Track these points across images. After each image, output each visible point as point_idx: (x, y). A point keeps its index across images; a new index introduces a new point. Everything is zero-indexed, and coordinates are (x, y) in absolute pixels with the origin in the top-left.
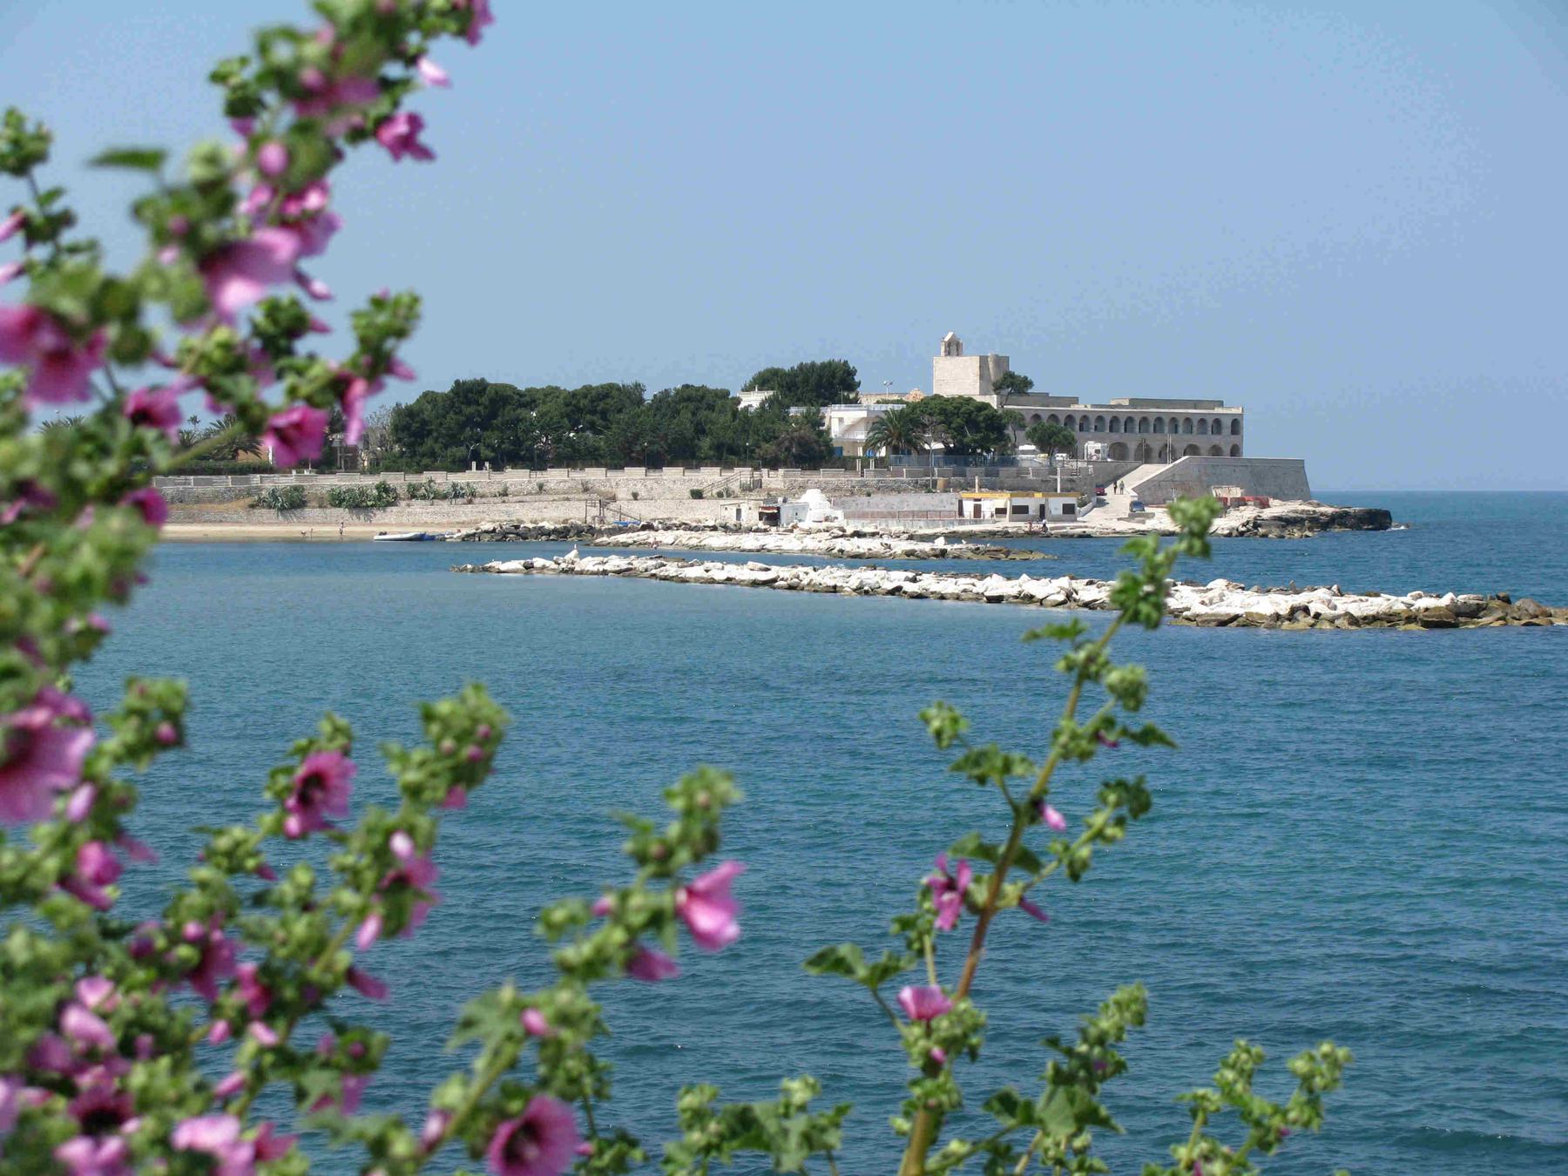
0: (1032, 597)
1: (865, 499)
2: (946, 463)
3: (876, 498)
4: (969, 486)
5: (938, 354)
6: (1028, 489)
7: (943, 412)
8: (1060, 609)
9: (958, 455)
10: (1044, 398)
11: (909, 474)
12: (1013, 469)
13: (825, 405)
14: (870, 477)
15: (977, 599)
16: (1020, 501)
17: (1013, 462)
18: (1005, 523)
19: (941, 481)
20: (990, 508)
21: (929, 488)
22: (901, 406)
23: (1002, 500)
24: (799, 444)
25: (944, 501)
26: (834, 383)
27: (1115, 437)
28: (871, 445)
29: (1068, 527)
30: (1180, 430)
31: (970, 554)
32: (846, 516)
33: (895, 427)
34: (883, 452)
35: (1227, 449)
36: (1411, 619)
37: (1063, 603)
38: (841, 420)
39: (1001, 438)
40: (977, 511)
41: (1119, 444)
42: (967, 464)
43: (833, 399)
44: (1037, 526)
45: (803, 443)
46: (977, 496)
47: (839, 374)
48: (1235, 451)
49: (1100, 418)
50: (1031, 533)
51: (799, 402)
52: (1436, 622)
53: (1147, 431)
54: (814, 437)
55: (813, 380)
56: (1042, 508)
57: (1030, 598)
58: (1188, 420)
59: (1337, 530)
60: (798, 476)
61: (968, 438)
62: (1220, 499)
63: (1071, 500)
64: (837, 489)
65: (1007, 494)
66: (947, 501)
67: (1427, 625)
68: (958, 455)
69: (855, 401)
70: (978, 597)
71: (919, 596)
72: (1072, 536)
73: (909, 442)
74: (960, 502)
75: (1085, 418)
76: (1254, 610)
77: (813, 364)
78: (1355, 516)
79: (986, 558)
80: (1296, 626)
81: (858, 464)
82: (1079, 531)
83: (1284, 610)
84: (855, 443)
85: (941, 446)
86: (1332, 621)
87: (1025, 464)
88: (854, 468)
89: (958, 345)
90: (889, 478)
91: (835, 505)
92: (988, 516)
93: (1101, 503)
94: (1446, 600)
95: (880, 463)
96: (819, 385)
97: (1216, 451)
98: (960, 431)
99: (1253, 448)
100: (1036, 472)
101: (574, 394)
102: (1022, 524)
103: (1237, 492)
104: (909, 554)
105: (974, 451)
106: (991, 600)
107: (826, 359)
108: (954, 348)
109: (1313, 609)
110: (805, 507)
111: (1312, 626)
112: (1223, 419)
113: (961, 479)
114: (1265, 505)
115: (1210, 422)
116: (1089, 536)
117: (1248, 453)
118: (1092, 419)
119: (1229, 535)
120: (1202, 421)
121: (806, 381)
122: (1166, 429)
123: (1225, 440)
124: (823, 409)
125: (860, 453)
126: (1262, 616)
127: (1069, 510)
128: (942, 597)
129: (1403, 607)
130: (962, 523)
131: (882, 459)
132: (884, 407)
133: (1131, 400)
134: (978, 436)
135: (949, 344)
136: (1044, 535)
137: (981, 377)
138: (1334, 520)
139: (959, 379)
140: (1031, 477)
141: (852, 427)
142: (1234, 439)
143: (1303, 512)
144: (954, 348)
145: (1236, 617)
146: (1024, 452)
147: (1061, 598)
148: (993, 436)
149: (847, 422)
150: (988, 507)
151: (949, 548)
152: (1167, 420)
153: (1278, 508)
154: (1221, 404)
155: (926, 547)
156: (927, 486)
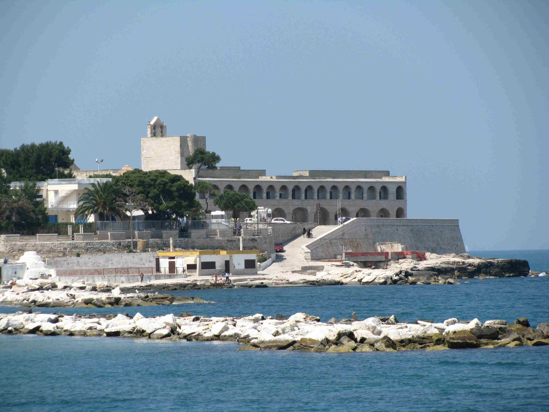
0: (144, 331)
1: (74, 259)
2: (147, 227)
3: (85, 258)
4: (164, 246)
5: (146, 136)
6: (215, 248)
7: (141, 183)
8: (164, 341)
9: (156, 221)
10: (236, 171)
11: (113, 237)
12: (203, 232)
13: (44, 180)
14: (80, 240)
15: (99, 335)
16: (208, 258)
17: (204, 225)
18: (196, 277)
19: (140, 243)
20: (182, 264)
21: (130, 248)
22: (110, 179)
23: (192, 257)
24: (19, 213)
25: (143, 259)
26: (52, 161)
27: (297, 203)
28: (81, 213)
29: (249, 279)
30: (353, 196)
31: (140, 301)
32: (59, 274)
33: (101, 197)
34: (91, 219)
35: (393, 212)
36: (439, 341)
37: (168, 335)
38: (56, 192)
39: (192, 205)
40: (172, 267)
41: (300, 209)
42: (163, 227)
43: (50, 175)
44: (221, 279)
45: (21, 212)
46: (172, 254)
47: (56, 153)
48: (400, 213)
49: (284, 188)
50: (216, 285)
51: (20, 178)
52: (460, 343)
53: (324, 198)
54: (32, 207)
55: (33, 159)
56: (227, 263)
57: (141, 333)
58: (359, 188)
59: (481, 277)
60: (18, 240)
61: (164, 206)
62: (382, 253)
63: (252, 256)
64: (51, 251)
65: (196, 253)
66: (145, 260)
67: (453, 346)
68: (156, 221)
69: (70, 176)
70: (100, 333)
71: (53, 334)
72: (251, 286)
73: (112, 209)
74: (157, 260)
75: (271, 187)
76: (307, 336)
77: (33, 146)
78: (498, 266)
79: (154, 304)
80: (342, 349)
81: (70, 229)
82: (258, 282)
83: (332, 337)
84: (68, 212)
85: (140, 213)
86: (372, 345)
87: (213, 227)
88: (66, 233)
89: (162, 127)
90: (96, 241)
91: (49, 265)
92: (180, 270)
93: (279, 259)
94: (473, 324)
95: (89, 228)
96: (38, 163)
97: (384, 213)
98: (156, 198)
99: (413, 212)
100: (223, 233)
101: (146, 173)
102: (209, 277)
103: (398, 248)
104: (88, 302)
105: (169, 218)
106: (109, 334)
107: (40, 143)
108: (158, 130)
109: (358, 335)
110: (23, 266)
111: (354, 349)
112: (388, 186)
113: (158, 240)
114: (421, 258)
115: (378, 188)
116: (265, 286)
117: (411, 214)
118: (277, 188)
119: (385, 283)
120: (372, 189)
121: (27, 159)
122: (341, 195)
123: (391, 204)
124: (39, 184)
125: (73, 220)
126: (313, 341)
127: (250, 264)
128: (71, 334)
129: (436, 331)
130: (157, 278)
131: (90, 224)
132: (92, 181)
133: (311, 172)
134: (172, 204)
135: (154, 127)
136: (229, 286)
137: (182, 154)
138: (479, 270)
139: (162, 156)
140: (218, 237)
141: (66, 198)
142: (399, 204)
143: (454, 262)
144: (158, 130)
145: (294, 342)
146: (217, 217)
147: (166, 332)
148: (184, 204)
149: (62, 194)
150: (181, 263)
151: (122, 296)
152: (341, 188)
153: (433, 260)
154: (387, 174)
155: (104, 296)
156: (128, 246)
